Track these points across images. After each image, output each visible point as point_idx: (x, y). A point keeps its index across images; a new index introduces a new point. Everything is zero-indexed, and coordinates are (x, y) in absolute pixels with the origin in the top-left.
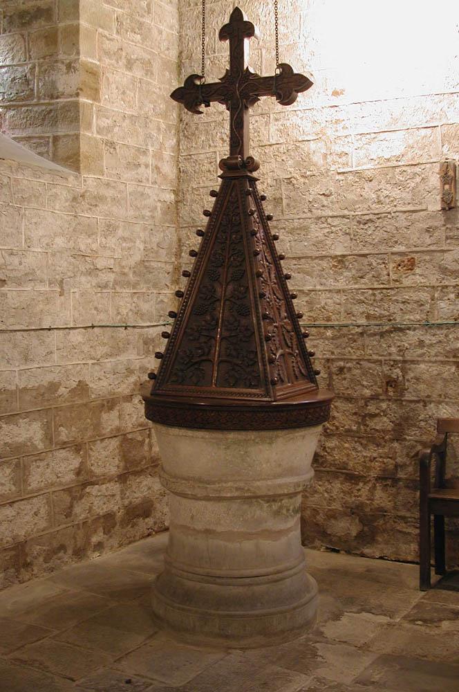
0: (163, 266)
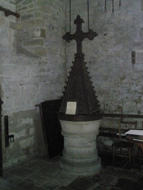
0: (63, 80)
